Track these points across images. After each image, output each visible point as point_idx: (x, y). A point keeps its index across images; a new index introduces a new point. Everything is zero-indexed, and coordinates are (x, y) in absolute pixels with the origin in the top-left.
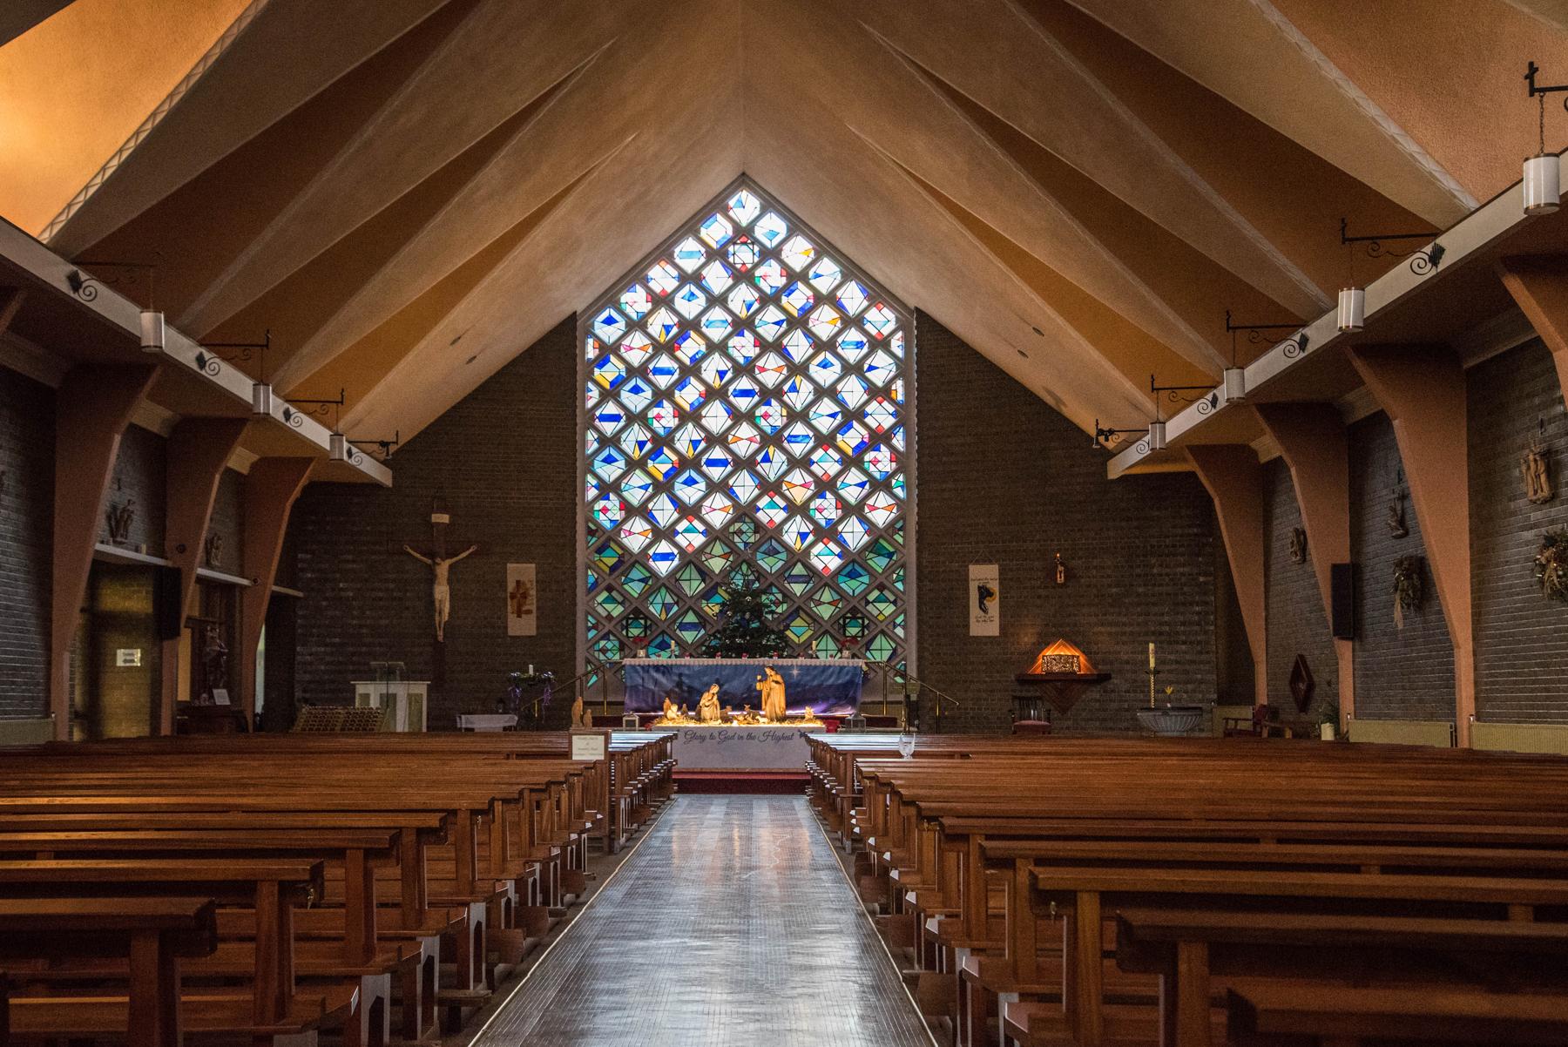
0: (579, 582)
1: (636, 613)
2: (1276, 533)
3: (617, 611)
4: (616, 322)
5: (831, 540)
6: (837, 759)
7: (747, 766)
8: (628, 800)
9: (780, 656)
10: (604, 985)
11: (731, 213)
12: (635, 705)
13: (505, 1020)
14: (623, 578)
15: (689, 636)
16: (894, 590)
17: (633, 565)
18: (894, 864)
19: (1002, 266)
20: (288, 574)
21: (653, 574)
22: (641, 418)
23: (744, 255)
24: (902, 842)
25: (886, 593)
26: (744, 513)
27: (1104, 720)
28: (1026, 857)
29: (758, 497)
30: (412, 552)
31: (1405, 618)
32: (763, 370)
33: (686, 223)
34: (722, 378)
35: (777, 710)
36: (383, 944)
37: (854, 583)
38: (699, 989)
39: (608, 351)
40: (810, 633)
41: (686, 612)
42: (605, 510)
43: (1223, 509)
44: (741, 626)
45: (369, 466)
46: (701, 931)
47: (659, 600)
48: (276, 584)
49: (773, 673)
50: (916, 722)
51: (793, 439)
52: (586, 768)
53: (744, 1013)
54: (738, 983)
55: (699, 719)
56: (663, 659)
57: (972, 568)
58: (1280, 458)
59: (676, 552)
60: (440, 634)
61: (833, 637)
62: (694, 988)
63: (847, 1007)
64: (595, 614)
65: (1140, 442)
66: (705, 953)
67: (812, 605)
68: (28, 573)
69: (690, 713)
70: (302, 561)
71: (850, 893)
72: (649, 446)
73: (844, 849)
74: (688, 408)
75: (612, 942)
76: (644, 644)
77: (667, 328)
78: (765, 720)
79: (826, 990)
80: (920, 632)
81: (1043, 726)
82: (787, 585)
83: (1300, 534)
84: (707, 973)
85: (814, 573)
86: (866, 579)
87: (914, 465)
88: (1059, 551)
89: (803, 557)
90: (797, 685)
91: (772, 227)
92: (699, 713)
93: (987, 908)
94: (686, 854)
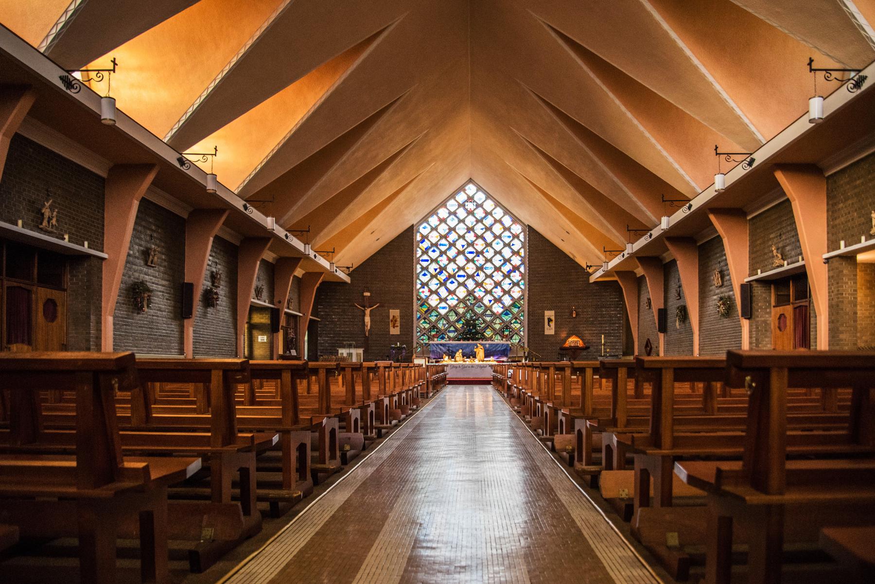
0: (414, 316)
1: (434, 327)
2: (641, 300)
3: (427, 326)
11: (466, 192)
12: (433, 357)
15: (452, 335)
17: (432, 311)
19: (556, 210)
20: (315, 313)
21: (439, 314)
22: (436, 261)
23: (470, 206)
25: (517, 320)
26: (470, 293)
31: (679, 325)
37: (507, 317)
39: (424, 238)
41: (450, 327)
42: (423, 292)
43: (625, 291)
45: (342, 276)
47: (441, 322)
48: (311, 316)
56: (443, 342)
58: (643, 275)
60: (367, 333)
68: (229, 308)
70: (320, 308)
72: (438, 270)
80: (528, 334)
83: (649, 299)
91: (480, 197)
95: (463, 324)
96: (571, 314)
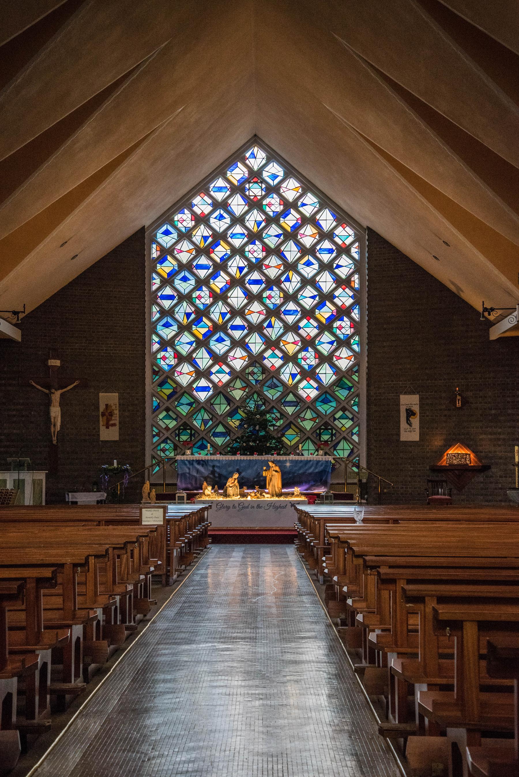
0: (147, 405)
3: (172, 424)
4: (171, 233)
5: (311, 378)
6: (314, 523)
7: (256, 525)
8: (179, 550)
9: (279, 454)
10: (162, 677)
12: (184, 486)
13: (95, 702)
14: (176, 403)
16: (352, 411)
17: (183, 395)
18: (349, 594)
21: (196, 400)
22: (188, 298)
24: (355, 581)
25: (347, 413)
27: (486, 495)
28: (432, 596)
29: (265, 351)
30: (35, 385)
32: (268, 267)
33: (219, 167)
34: (241, 272)
35: (276, 489)
36: (13, 657)
37: (326, 407)
38: (223, 677)
40: (298, 439)
41: (217, 425)
42: (164, 358)
44: (253, 435)
46: (226, 638)
47: (199, 417)
49: (274, 465)
50: (366, 496)
51: (288, 312)
52: (151, 531)
53: (252, 694)
54: (248, 673)
55: (226, 495)
56: (202, 455)
57: (402, 397)
59: (211, 386)
60: (55, 439)
61: (313, 442)
62: (220, 677)
63: (319, 689)
64: (157, 426)
65: (511, 316)
66: (228, 653)
67: (299, 421)
69: (220, 491)
71: (323, 611)
72: (193, 316)
73: (319, 581)
74: (218, 291)
75: (167, 646)
76: (190, 446)
77: (205, 238)
78: (269, 496)
79: (305, 677)
81: (446, 499)
82: (283, 408)
84: (229, 667)
85: (300, 399)
86: (334, 404)
87: (366, 330)
88: (458, 386)
89: (293, 390)
90: (289, 473)
92: (226, 491)
93: (408, 625)
94: (217, 585)
95: (241, 420)
96: (453, 401)
